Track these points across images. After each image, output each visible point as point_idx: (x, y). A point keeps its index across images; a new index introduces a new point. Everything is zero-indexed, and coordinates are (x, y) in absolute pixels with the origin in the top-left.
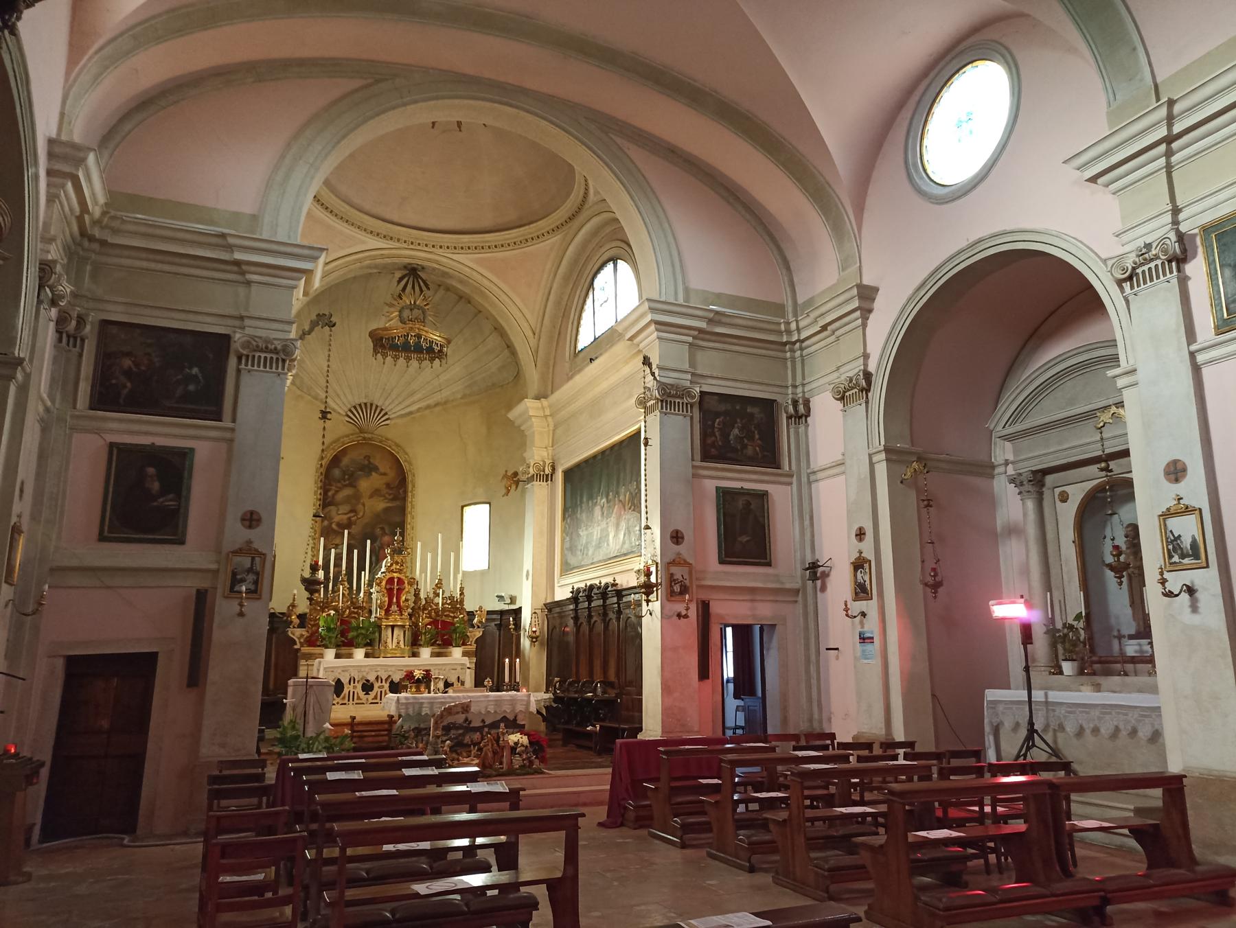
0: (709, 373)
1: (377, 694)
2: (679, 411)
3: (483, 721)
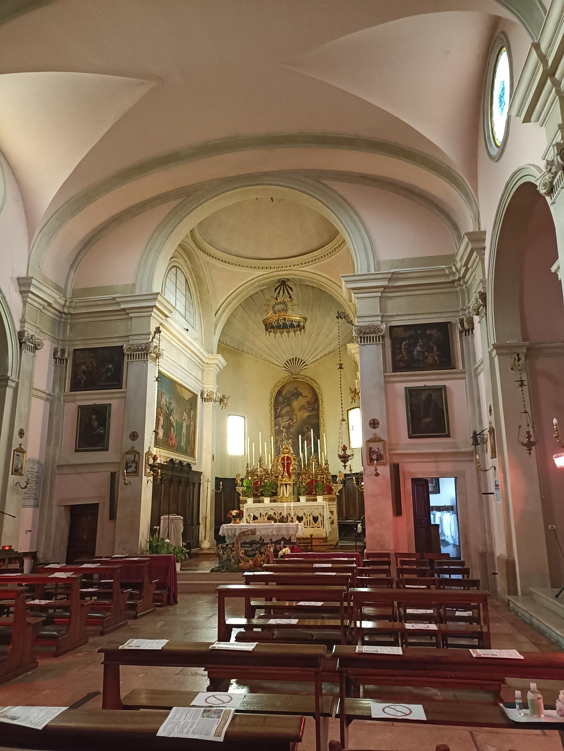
0: (395, 313)
1: (305, 522)
2: (373, 342)
3: (271, 540)
